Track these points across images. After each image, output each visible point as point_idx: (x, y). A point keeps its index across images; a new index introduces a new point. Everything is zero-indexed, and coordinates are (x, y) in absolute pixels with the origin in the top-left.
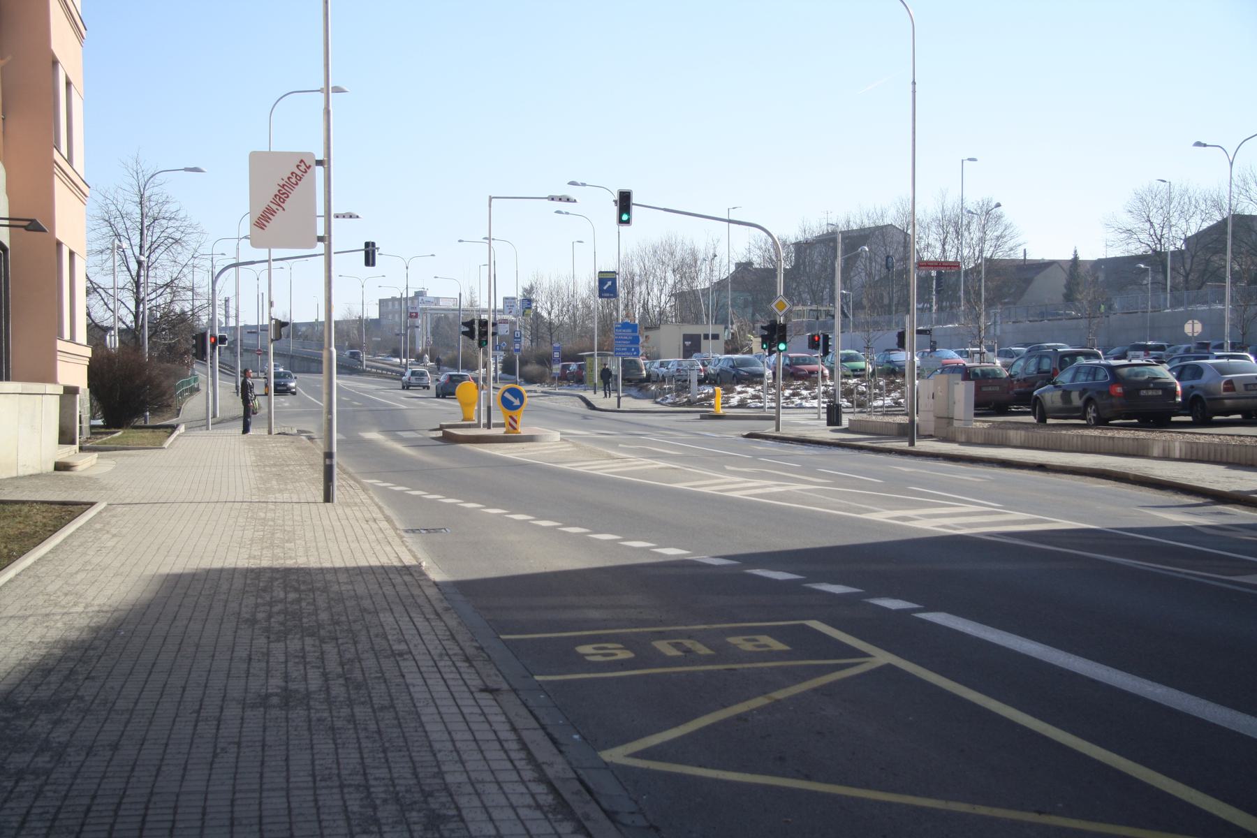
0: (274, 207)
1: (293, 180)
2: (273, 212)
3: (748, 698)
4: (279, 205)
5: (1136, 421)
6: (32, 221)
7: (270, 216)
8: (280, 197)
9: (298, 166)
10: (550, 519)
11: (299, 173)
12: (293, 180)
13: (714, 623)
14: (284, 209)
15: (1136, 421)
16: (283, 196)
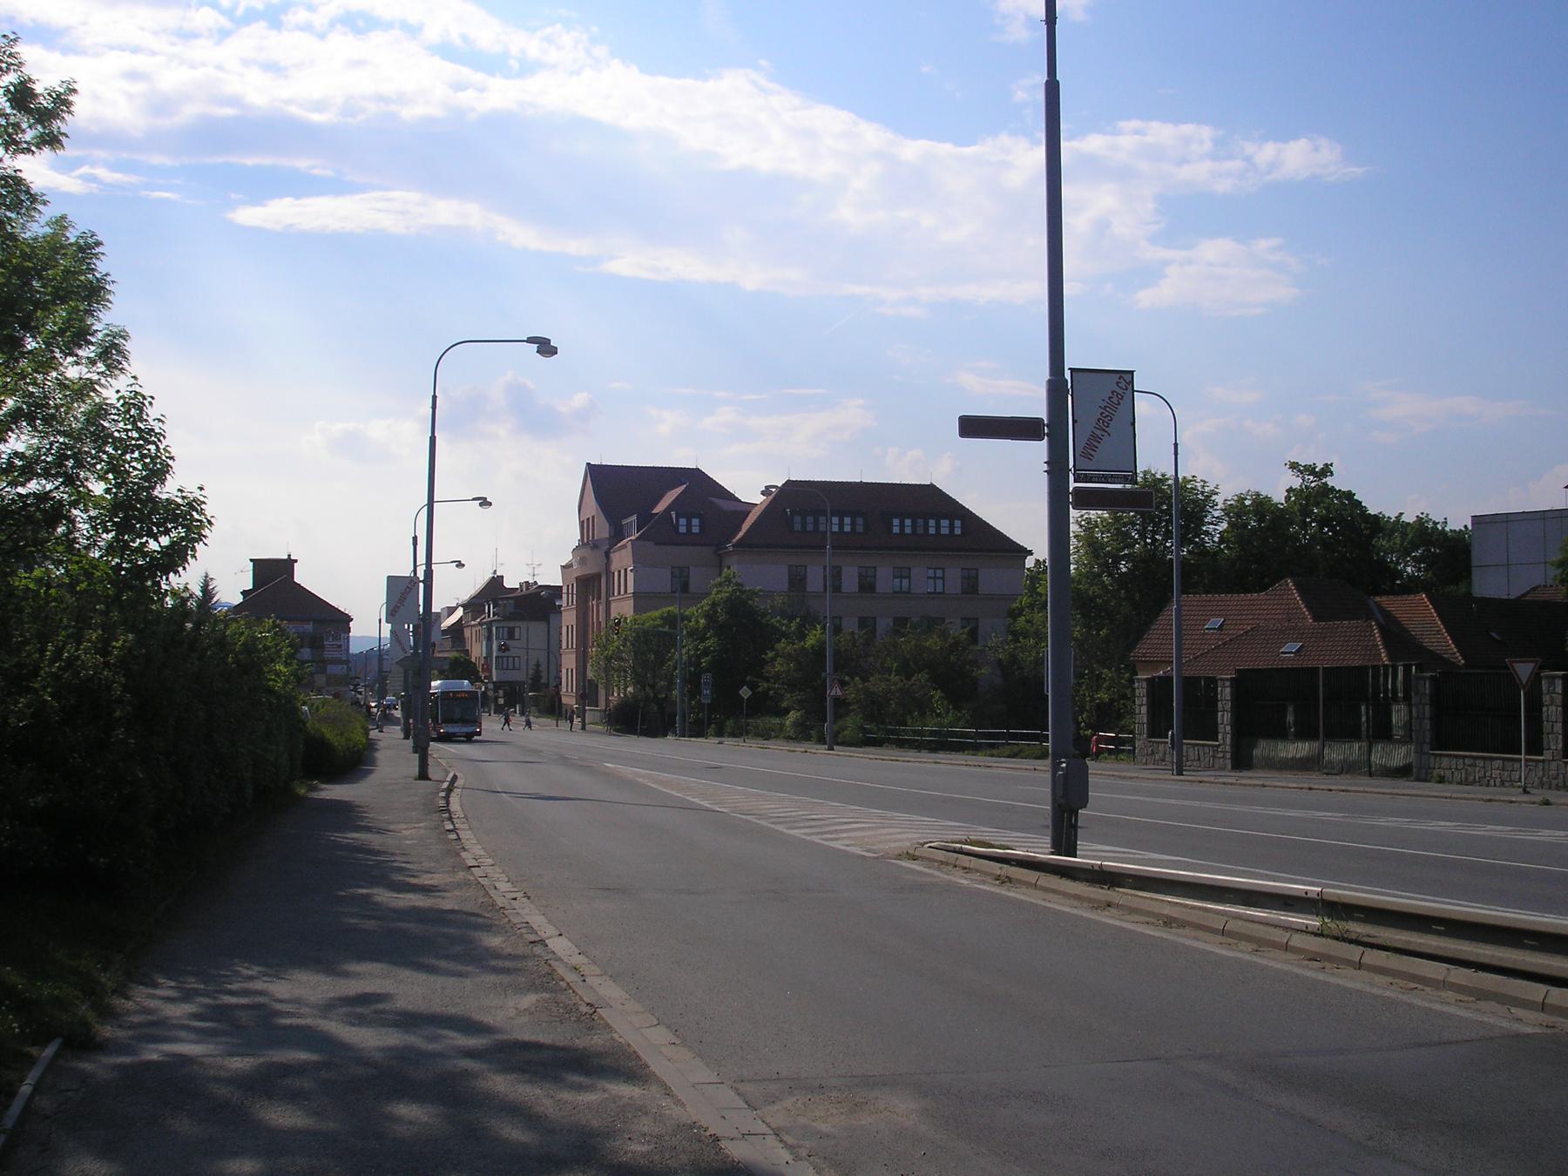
0: (1099, 433)
1: (1115, 400)
2: (1098, 439)
3: (1297, 976)
4: (1104, 430)
5: (1443, 928)
6: (460, 562)
7: (1096, 444)
8: (1103, 421)
9: (1117, 383)
10: (607, 767)
11: (1120, 391)
12: (1115, 400)
13: (1376, 887)
14: (1109, 435)
15: (1443, 928)
16: (1106, 420)
